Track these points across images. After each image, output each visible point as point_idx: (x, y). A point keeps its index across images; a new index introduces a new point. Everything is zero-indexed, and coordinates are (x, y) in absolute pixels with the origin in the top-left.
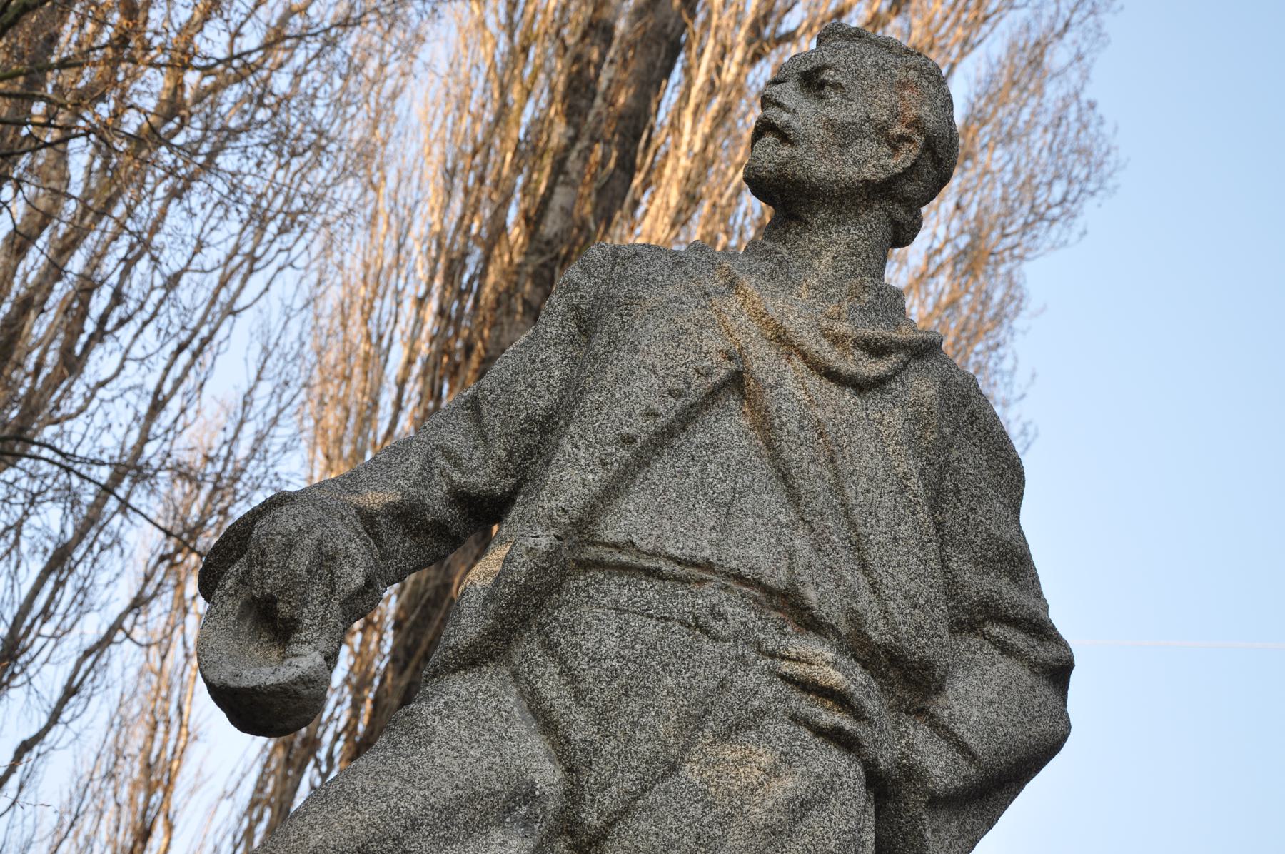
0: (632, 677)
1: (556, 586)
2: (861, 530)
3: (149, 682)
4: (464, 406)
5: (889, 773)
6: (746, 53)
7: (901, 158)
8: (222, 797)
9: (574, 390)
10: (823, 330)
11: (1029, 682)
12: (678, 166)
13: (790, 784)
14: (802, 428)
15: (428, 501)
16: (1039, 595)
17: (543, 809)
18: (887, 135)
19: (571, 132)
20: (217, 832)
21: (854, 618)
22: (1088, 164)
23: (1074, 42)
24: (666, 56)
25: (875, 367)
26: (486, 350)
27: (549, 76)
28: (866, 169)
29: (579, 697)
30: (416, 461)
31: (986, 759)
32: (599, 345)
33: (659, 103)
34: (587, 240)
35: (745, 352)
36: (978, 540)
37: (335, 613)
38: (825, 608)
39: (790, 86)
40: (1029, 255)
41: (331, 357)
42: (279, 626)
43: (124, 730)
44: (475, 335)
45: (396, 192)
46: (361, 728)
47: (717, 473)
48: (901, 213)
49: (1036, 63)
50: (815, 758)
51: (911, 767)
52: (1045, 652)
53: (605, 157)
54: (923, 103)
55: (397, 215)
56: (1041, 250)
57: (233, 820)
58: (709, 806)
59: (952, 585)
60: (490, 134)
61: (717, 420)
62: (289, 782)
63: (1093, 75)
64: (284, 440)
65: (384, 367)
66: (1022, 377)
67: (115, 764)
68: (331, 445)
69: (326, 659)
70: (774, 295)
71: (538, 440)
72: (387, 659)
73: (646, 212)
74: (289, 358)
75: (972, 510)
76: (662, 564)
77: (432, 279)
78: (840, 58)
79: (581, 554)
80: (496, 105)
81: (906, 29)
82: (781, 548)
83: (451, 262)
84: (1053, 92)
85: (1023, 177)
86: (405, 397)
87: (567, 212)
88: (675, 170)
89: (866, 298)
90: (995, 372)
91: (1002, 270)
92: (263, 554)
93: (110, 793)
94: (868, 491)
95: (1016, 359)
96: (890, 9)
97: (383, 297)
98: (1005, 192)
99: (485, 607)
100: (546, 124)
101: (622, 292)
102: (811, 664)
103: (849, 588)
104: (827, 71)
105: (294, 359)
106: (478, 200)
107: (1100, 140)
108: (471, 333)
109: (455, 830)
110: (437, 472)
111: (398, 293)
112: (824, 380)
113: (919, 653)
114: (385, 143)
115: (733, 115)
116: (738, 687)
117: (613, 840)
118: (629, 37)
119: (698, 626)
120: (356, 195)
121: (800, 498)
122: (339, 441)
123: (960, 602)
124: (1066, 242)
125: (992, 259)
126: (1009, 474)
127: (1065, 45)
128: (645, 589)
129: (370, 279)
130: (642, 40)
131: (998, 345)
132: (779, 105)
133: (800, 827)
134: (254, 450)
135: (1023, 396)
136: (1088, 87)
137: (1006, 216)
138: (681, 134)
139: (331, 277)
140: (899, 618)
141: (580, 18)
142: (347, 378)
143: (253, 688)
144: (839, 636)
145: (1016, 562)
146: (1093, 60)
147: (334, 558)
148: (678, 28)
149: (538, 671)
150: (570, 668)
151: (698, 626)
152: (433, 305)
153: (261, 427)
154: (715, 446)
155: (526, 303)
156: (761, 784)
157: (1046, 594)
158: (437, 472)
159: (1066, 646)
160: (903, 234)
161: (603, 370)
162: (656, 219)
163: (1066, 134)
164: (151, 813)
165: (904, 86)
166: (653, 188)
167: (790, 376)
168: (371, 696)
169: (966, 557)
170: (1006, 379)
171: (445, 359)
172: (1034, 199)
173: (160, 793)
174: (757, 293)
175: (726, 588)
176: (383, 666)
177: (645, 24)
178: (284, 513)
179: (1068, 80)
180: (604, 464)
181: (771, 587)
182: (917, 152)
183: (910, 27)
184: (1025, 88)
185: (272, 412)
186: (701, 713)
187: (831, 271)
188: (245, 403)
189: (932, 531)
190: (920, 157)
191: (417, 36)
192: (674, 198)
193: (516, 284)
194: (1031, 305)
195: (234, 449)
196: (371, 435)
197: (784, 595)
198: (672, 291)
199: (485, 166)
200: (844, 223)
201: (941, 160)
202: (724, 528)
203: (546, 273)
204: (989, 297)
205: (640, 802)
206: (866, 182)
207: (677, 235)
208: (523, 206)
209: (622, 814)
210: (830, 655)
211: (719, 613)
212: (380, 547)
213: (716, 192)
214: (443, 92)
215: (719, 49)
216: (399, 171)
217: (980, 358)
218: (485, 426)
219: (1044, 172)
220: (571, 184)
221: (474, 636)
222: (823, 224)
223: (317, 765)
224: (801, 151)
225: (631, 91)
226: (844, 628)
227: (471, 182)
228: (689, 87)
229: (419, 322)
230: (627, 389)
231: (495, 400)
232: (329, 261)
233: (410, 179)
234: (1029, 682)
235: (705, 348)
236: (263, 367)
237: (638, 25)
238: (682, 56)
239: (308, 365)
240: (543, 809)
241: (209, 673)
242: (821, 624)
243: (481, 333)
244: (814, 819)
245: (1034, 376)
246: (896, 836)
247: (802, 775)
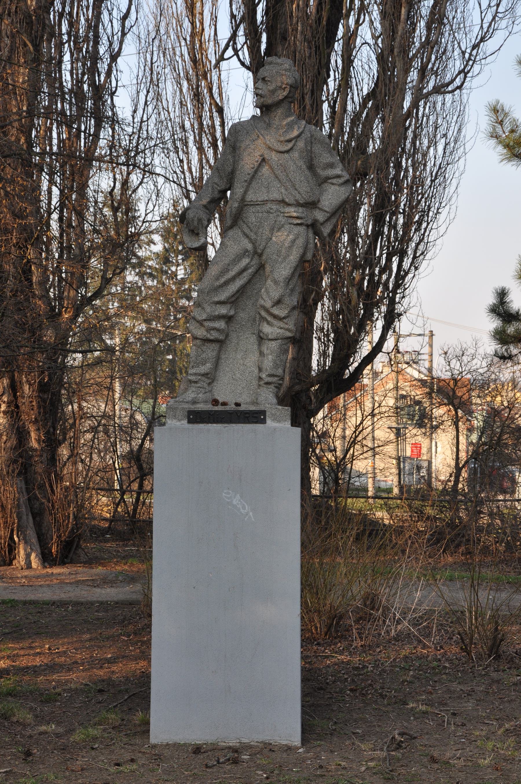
1: (242, 210)
21: (296, 200)
119: (268, 212)
151: (268, 212)
165: (283, 75)
202: (268, 192)
244: (297, 242)
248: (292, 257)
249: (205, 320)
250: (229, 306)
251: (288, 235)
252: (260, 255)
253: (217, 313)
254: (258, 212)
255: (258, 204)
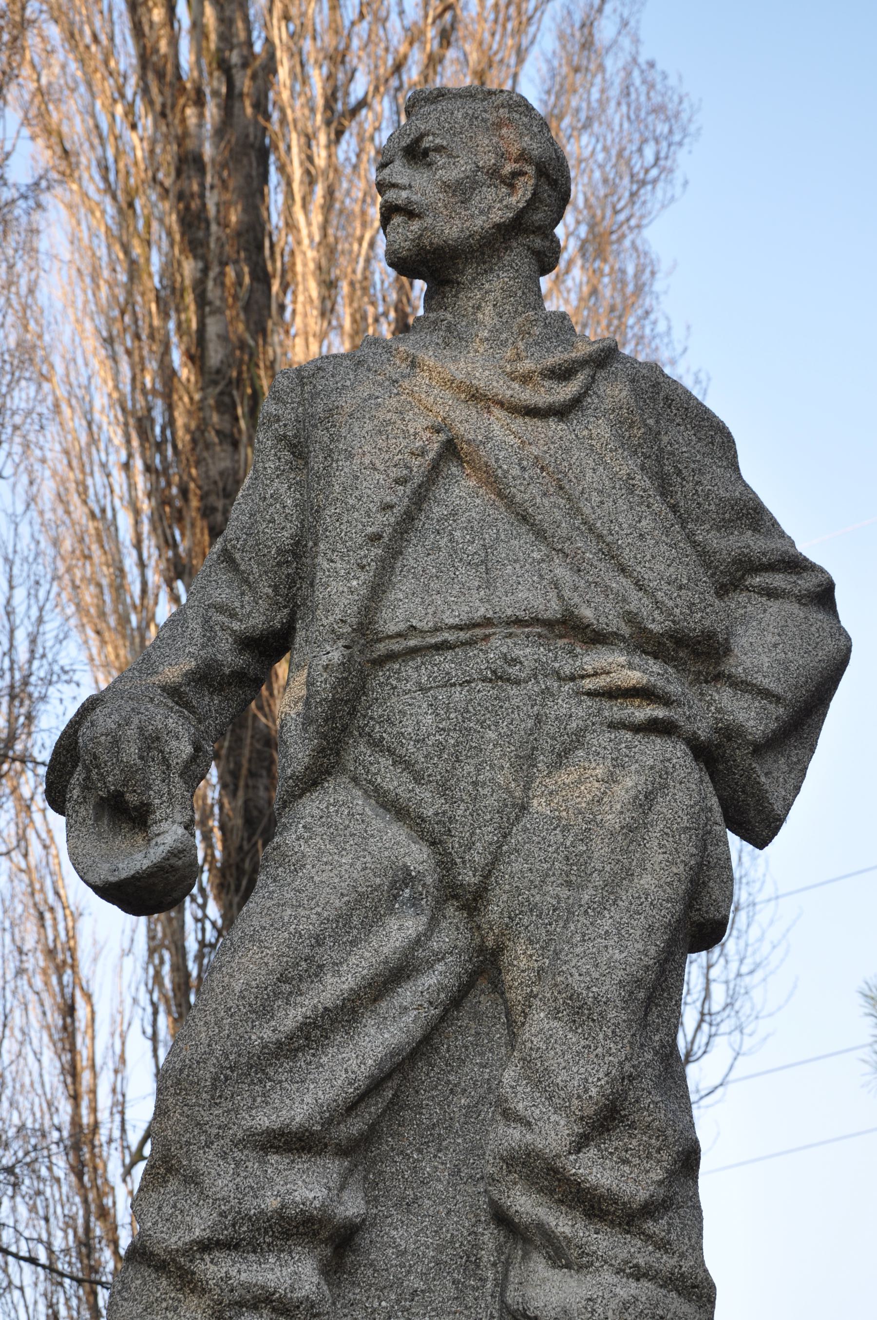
0: (457, 744)
1: (362, 690)
2: (609, 539)
3: (21, 881)
4: (219, 561)
5: (710, 741)
6: (329, 135)
7: (520, 193)
8: (122, 956)
9: (310, 514)
10: (509, 374)
11: (802, 615)
12: (306, 260)
13: (630, 783)
14: (524, 469)
15: (220, 657)
16: (782, 535)
17: (424, 885)
18: (500, 176)
19: (200, 265)
20: (129, 986)
21: (631, 618)
22: (667, 119)
23: (615, 11)
24: (258, 165)
25: (568, 390)
26: (199, 487)
27: (161, 221)
28: (492, 213)
29: (418, 779)
30: (195, 625)
31: (789, 695)
32: (317, 462)
33: (268, 209)
34: (251, 355)
35: (448, 421)
36: (713, 507)
37: (178, 786)
38: (603, 620)
39: (397, 164)
40: (645, 222)
41: (67, 544)
42: (134, 814)
43: (16, 930)
44: (185, 478)
45: (68, 375)
46: (218, 854)
47: (464, 537)
48: (538, 243)
49: (587, 44)
50: (643, 753)
51: (727, 728)
52: (806, 583)
53: (239, 276)
54: (521, 135)
55: (76, 397)
56: (654, 213)
57: (140, 972)
58: (566, 829)
59: (705, 556)
60: (130, 293)
61: (447, 491)
62: (175, 923)
63: (643, 35)
64: (54, 633)
65: (117, 536)
66: (678, 333)
67: (21, 961)
68: (97, 621)
69: (186, 828)
70: (455, 360)
71: (295, 568)
72: (218, 788)
73: (294, 312)
74: (31, 559)
75: (698, 483)
76: (446, 636)
77: (128, 441)
78: (432, 122)
79: (371, 654)
80: (125, 265)
81: (462, 58)
82: (545, 582)
83: (140, 420)
84: (613, 65)
85: (614, 152)
86: (145, 555)
87: (224, 338)
88: (305, 265)
89: (536, 330)
90: (654, 338)
91: (627, 243)
92: (95, 757)
93: (26, 987)
94: (602, 502)
95: (668, 319)
96: (441, 45)
97: (92, 474)
98: (603, 173)
99: (306, 731)
100: (176, 266)
101: (319, 408)
102: (608, 673)
103: (617, 594)
104: (426, 139)
105: (35, 559)
106: (142, 358)
107: (670, 93)
108: (181, 478)
109: (355, 932)
110: (217, 628)
111: (104, 466)
112: (527, 419)
113: (699, 627)
114: (40, 337)
115: (338, 194)
116: (553, 717)
117: (493, 890)
118: (219, 159)
119: (498, 678)
120: (32, 394)
121: (545, 531)
122: (102, 615)
123: (717, 568)
124: (673, 197)
125: (614, 237)
126: (718, 439)
127: (608, 17)
128: (440, 663)
129: (75, 463)
130: (231, 157)
131: (647, 313)
132: (394, 186)
133: (652, 816)
134: (32, 652)
135: (685, 350)
136: (642, 49)
137: (612, 194)
138: (299, 231)
139: (39, 474)
140: (671, 604)
141: (169, 158)
142: (88, 557)
143: (133, 876)
144: (623, 639)
145: (753, 514)
146: (638, 21)
147: (158, 738)
148: (259, 134)
149: (373, 769)
150: (400, 756)
151: (498, 678)
152: (138, 464)
153: (30, 629)
154: (454, 514)
155: (218, 433)
156: (605, 793)
157: (788, 532)
158: (217, 628)
159: (822, 571)
160: (547, 259)
161: (330, 484)
162: (305, 315)
163: (637, 99)
164: (68, 991)
165: (499, 125)
166: (292, 287)
167: (496, 427)
168: (216, 824)
169: (707, 526)
170: (666, 340)
171: (167, 509)
172: (631, 169)
173: (69, 971)
174: (439, 364)
175: (510, 635)
176: (216, 795)
177: (229, 142)
178: (99, 715)
179: (622, 49)
180: (363, 567)
181: (549, 620)
182: (532, 182)
183: (465, 55)
184: (587, 69)
185: (34, 612)
186: (529, 752)
187: (496, 318)
188: (8, 614)
189: (671, 516)
190: (536, 185)
191: (32, 231)
192: (314, 289)
193: (204, 419)
194: (663, 267)
195: (15, 657)
196: (128, 600)
197: (563, 622)
198: (364, 390)
199: (136, 321)
200: (491, 270)
201: (556, 181)
202: (488, 584)
203: (226, 399)
204: (623, 272)
205: (505, 848)
206: (498, 226)
207: (330, 323)
208: (183, 347)
209: (493, 863)
210: (622, 659)
211: (513, 660)
212: (194, 713)
213: (349, 270)
214: (74, 273)
215: (303, 140)
216: (63, 357)
217: (636, 329)
218: (244, 572)
219: (631, 141)
220: (218, 311)
221: (306, 760)
222: (474, 279)
223: (194, 900)
224: (429, 220)
225: (239, 208)
226: (626, 630)
227: (129, 343)
228: (289, 184)
229: (132, 486)
230: (357, 493)
231: (244, 546)
232: (32, 460)
233: (74, 360)
234: (802, 615)
235: (412, 431)
236: (11, 576)
237: (223, 145)
238: (272, 158)
239: (48, 559)
240: (424, 885)
241: (90, 877)
242: (604, 635)
243: (190, 474)
244: (661, 805)
245: (688, 328)
246: (735, 791)
247: (637, 772)
248: (647, 881)
249: (206, 1246)
250: (334, 1166)
251: (611, 779)
252: (472, 902)
253: (272, 1203)
254: (448, 684)
255: (442, 647)
